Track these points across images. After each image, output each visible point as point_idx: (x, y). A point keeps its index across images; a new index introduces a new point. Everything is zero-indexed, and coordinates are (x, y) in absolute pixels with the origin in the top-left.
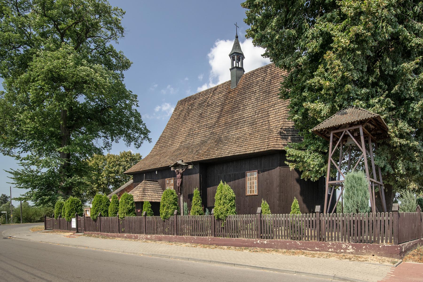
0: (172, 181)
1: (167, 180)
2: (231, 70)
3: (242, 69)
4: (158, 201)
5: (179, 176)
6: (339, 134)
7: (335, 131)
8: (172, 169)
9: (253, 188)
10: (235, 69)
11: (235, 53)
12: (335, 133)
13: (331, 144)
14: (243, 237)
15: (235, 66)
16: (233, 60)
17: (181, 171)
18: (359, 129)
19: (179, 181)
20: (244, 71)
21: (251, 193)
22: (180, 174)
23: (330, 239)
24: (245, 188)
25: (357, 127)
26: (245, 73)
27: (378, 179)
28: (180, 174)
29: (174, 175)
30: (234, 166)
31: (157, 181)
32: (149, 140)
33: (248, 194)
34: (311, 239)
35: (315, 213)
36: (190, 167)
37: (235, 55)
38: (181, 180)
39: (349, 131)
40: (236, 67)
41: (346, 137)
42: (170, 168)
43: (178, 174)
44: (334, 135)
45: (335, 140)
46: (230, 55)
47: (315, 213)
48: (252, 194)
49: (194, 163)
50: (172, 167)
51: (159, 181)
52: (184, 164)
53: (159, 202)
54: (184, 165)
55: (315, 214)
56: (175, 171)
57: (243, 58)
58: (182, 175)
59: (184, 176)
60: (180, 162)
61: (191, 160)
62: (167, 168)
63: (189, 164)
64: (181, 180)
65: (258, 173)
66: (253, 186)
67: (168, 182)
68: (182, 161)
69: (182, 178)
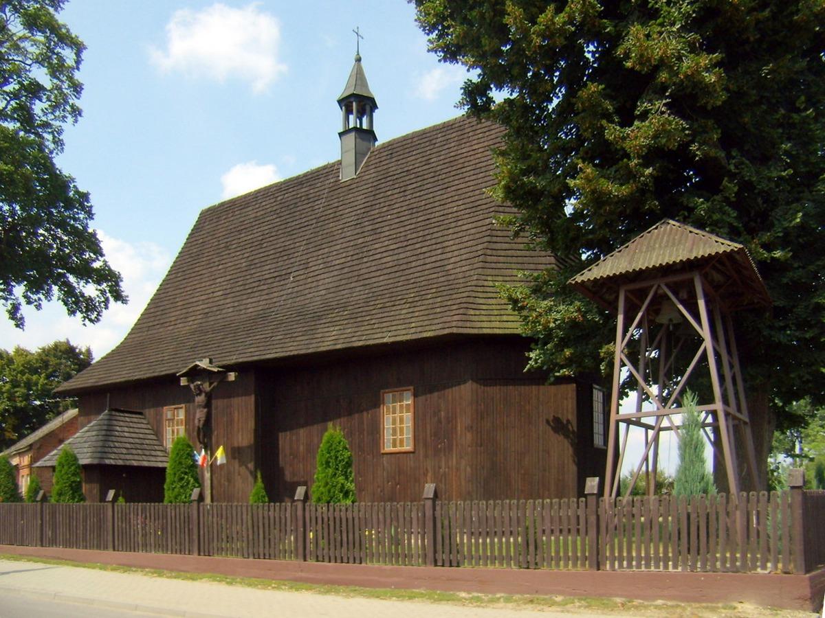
0: (181, 415)
1: (168, 411)
2: (341, 135)
3: (370, 135)
4: (160, 465)
5: (201, 399)
6: (642, 294)
7: (632, 286)
8: (183, 382)
9: (402, 434)
10: (352, 135)
11: (353, 95)
12: (632, 292)
13: (620, 319)
14: (372, 561)
15: (351, 126)
16: (349, 111)
17: (207, 387)
18: (692, 281)
19: (200, 414)
20: (376, 139)
21: (394, 446)
22: (203, 395)
23: (625, 563)
24: (378, 432)
25: (686, 276)
26: (377, 144)
27: (739, 410)
28: (203, 395)
29: (185, 396)
30: (354, 376)
31: (141, 413)
32: (468, 70)
33: (388, 448)
34: (639, 566)
35: (585, 496)
36: (232, 376)
37: (352, 99)
38: (206, 410)
39: (667, 285)
40: (355, 129)
41: (660, 300)
42: (178, 379)
43: (199, 394)
44: (629, 295)
45: (684, 295)
46: (340, 102)
47: (585, 496)
48: (398, 449)
49: (240, 368)
50: (183, 375)
51: (147, 412)
52: (216, 370)
53: (164, 469)
54: (214, 372)
55: (584, 499)
56: (192, 386)
57: (374, 106)
58: (209, 397)
59: (214, 402)
60: (204, 364)
61: (233, 359)
62: (172, 379)
63: (229, 368)
64: (206, 410)
65: (415, 395)
66: (402, 429)
67: (169, 415)
68: (211, 362)
69: (208, 405)
